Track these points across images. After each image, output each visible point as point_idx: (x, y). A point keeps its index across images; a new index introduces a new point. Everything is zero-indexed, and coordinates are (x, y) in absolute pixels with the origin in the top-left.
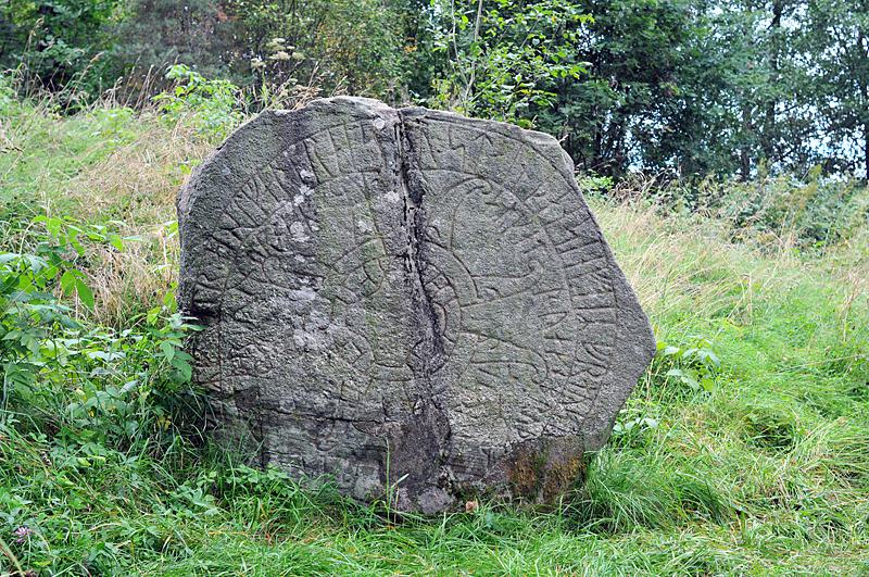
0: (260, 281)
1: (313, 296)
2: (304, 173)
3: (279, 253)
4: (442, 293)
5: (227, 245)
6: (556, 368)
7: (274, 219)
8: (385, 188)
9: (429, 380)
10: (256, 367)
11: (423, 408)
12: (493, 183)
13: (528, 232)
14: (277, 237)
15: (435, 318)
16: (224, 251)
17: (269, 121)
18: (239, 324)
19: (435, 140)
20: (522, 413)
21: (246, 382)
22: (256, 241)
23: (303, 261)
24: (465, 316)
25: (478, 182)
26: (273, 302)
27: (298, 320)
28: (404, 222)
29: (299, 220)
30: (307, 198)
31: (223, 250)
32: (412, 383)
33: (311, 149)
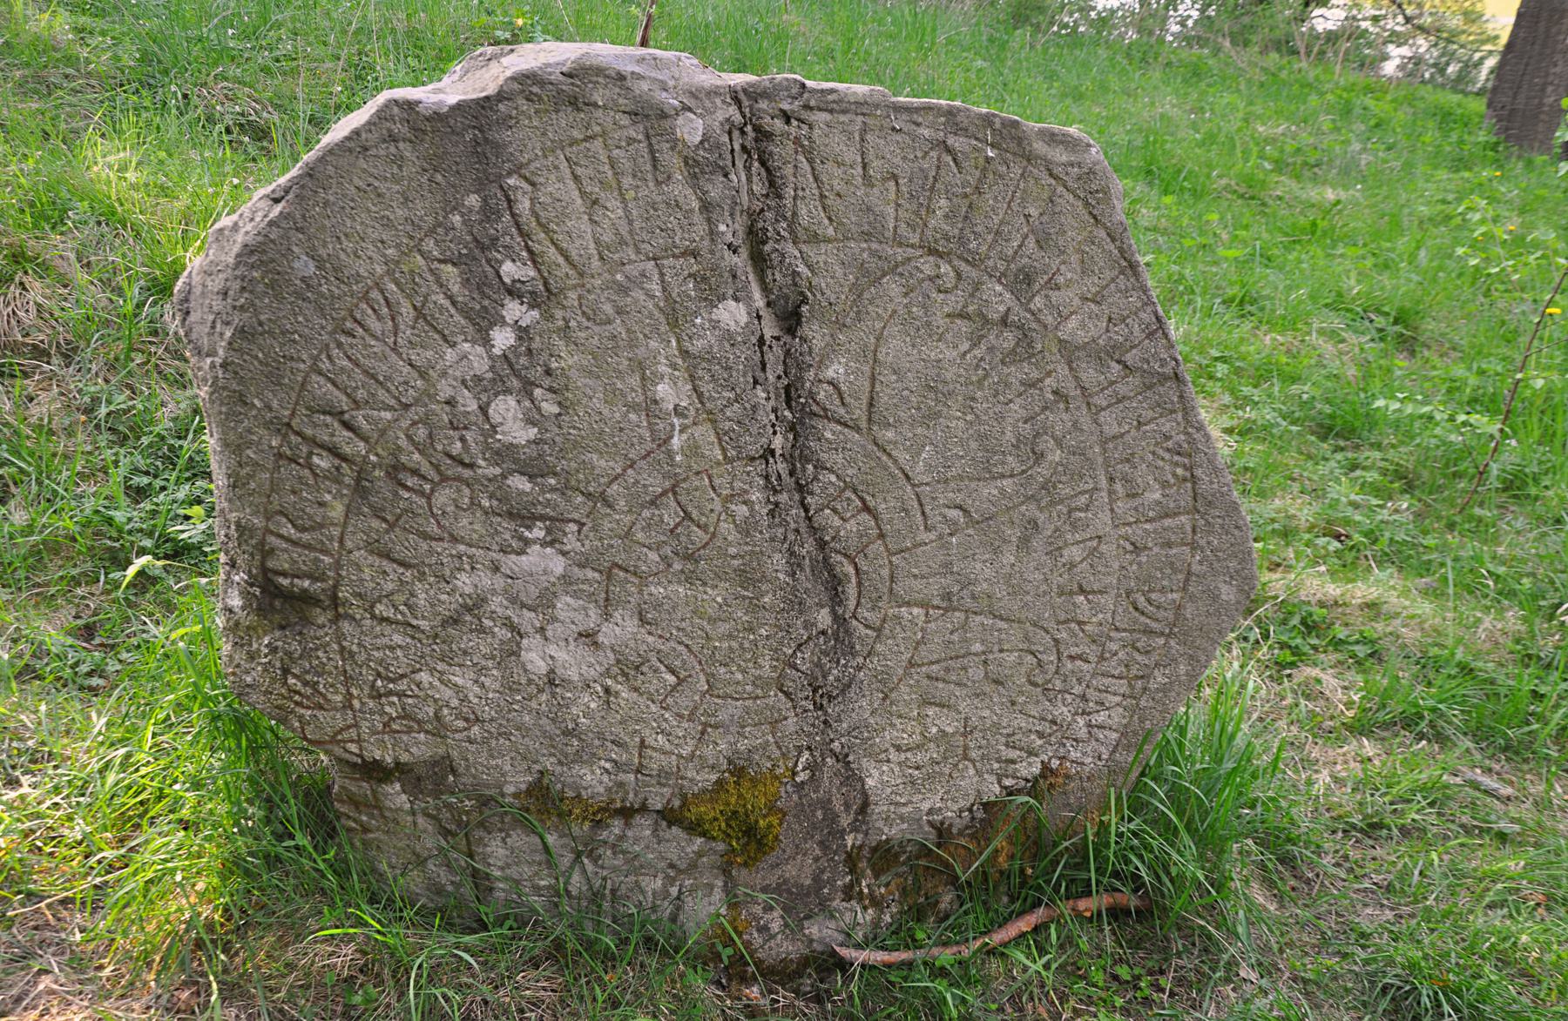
0: (425, 536)
1: (558, 565)
2: (509, 270)
3: (467, 473)
4: (848, 527)
5: (334, 451)
6: (1074, 651)
7: (445, 390)
8: (712, 298)
9: (826, 713)
10: (437, 717)
11: (812, 767)
12: (963, 266)
13: (1035, 375)
14: (456, 434)
15: (834, 588)
16: (323, 464)
17: (399, 128)
18: (388, 630)
19: (829, 165)
20: (1007, 745)
21: (419, 748)
22: (403, 442)
23: (527, 487)
24: (900, 574)
25: (927, 265)
26: (464, 582)
27: (528, 620)
28: (759, 374)
29: (508, 391)
30: (523, 333)
31: (322, 462)
32: (791, 723)
33: (524, 205)
